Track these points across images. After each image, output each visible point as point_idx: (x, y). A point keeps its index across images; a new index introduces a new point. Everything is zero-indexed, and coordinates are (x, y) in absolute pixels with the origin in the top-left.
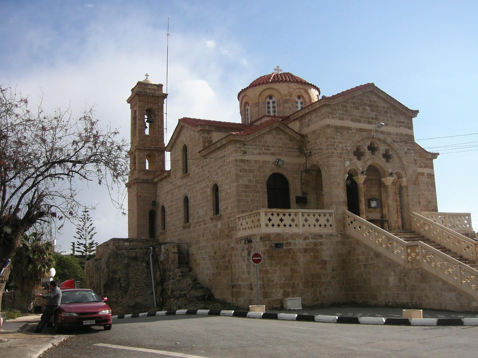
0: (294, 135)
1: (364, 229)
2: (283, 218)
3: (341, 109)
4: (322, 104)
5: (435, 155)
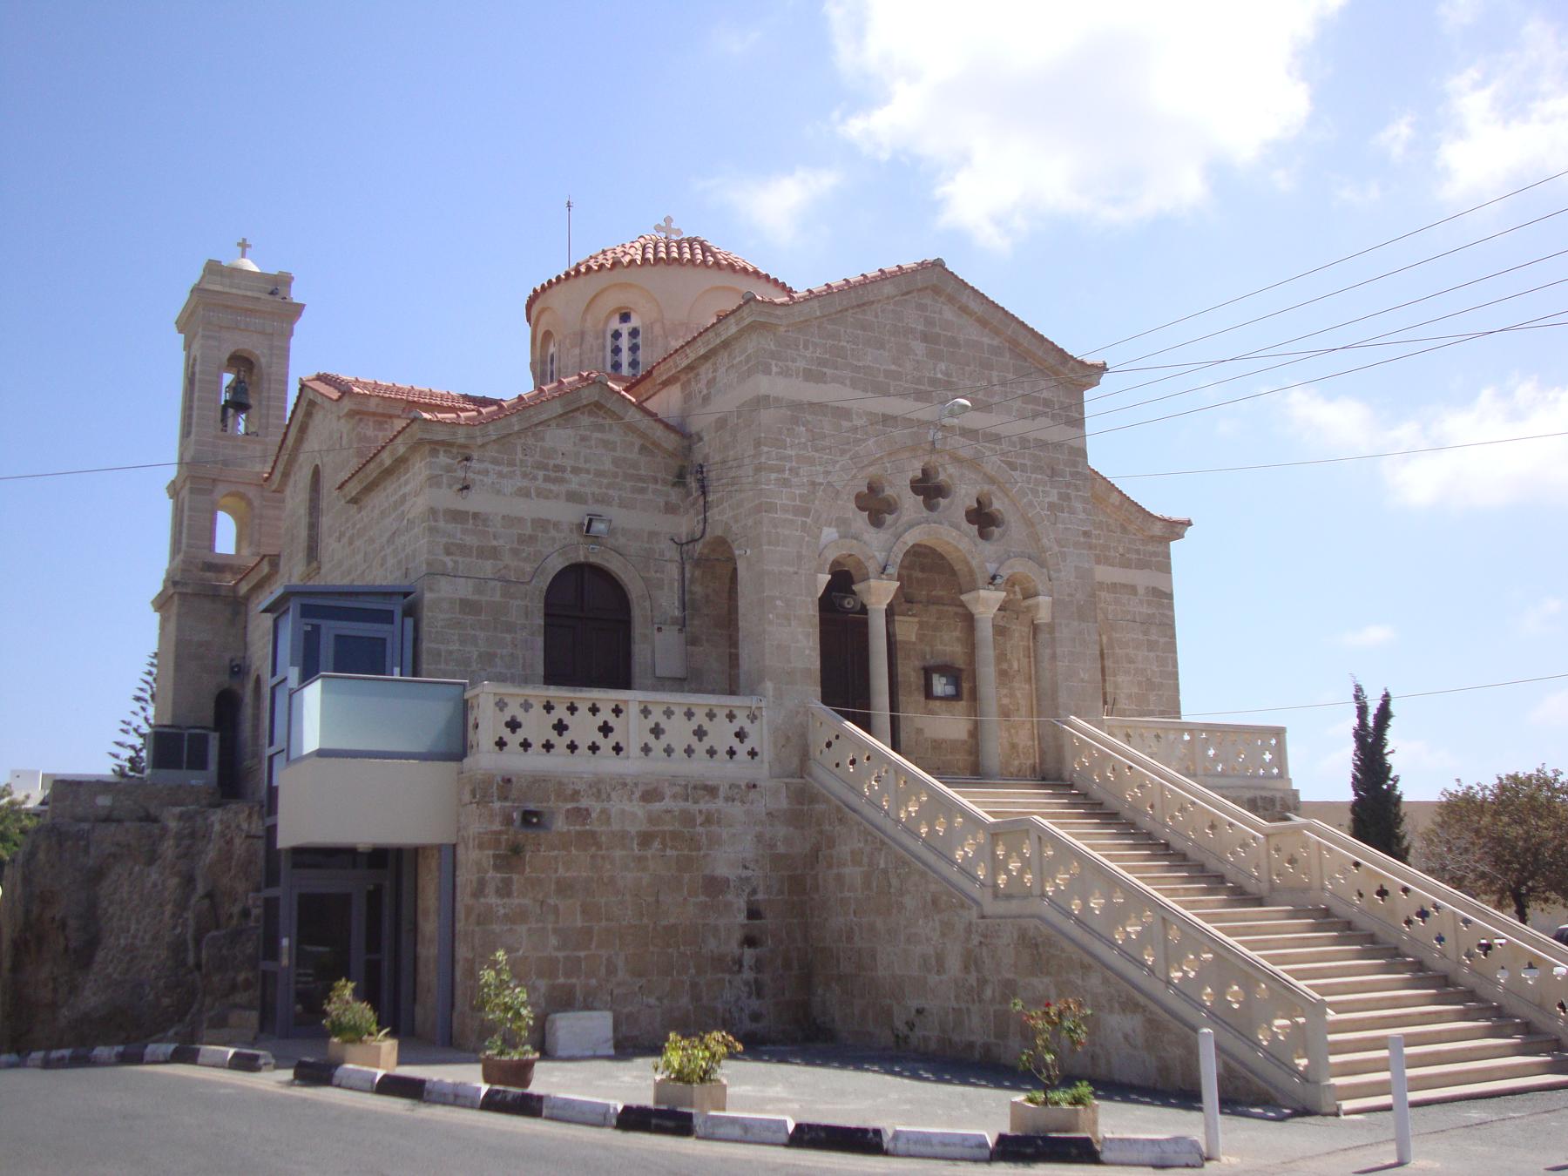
0: (659, 432)
1: (877, 771)
2: (664, 723)
3: (816, 345)
4: (747, 322)
5: (1176, 528)
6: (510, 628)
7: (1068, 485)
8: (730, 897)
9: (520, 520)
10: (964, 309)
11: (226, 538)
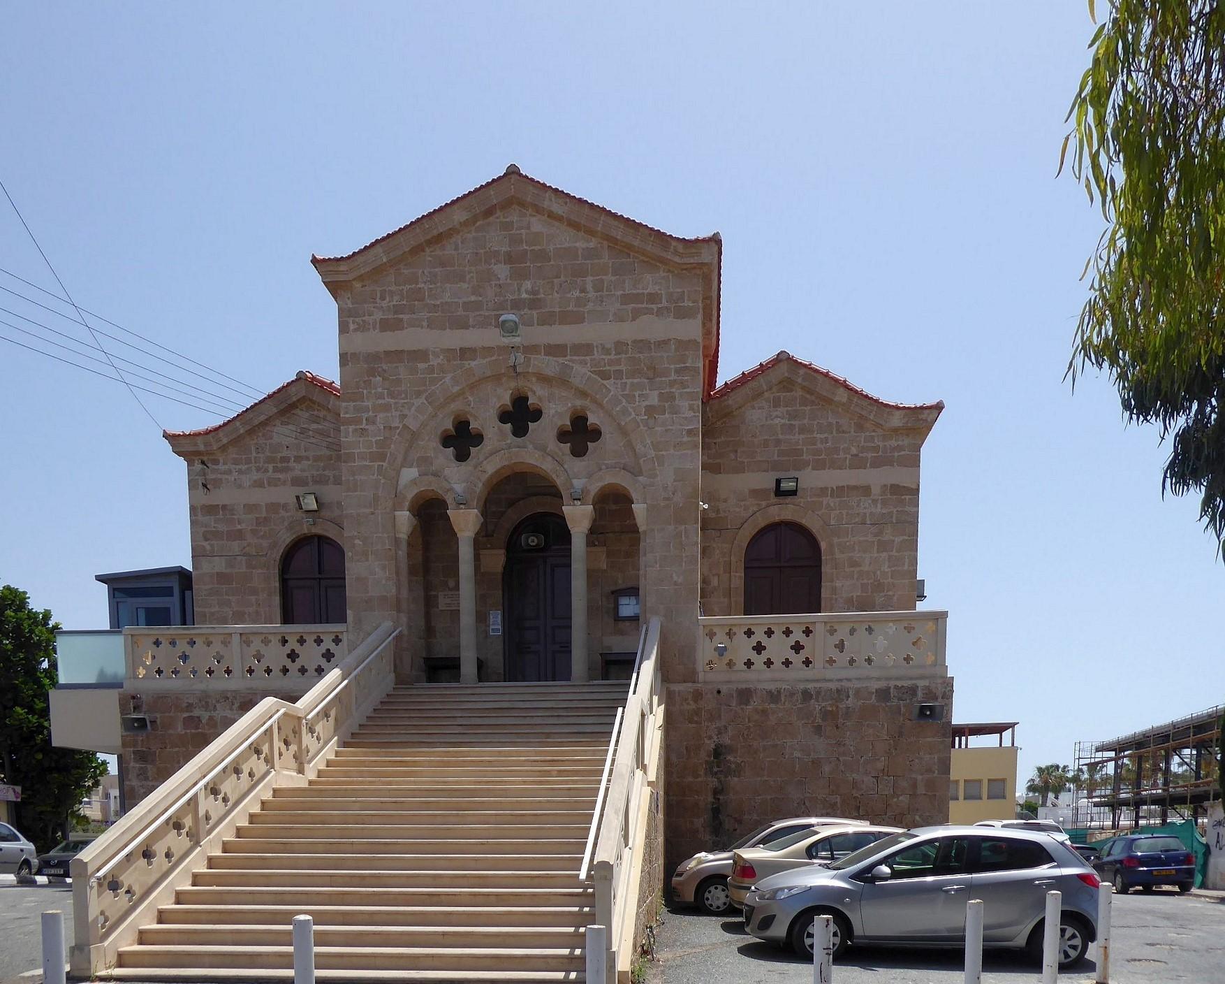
3: (392, 293)
5: (921, 420)
6: (254, 592)
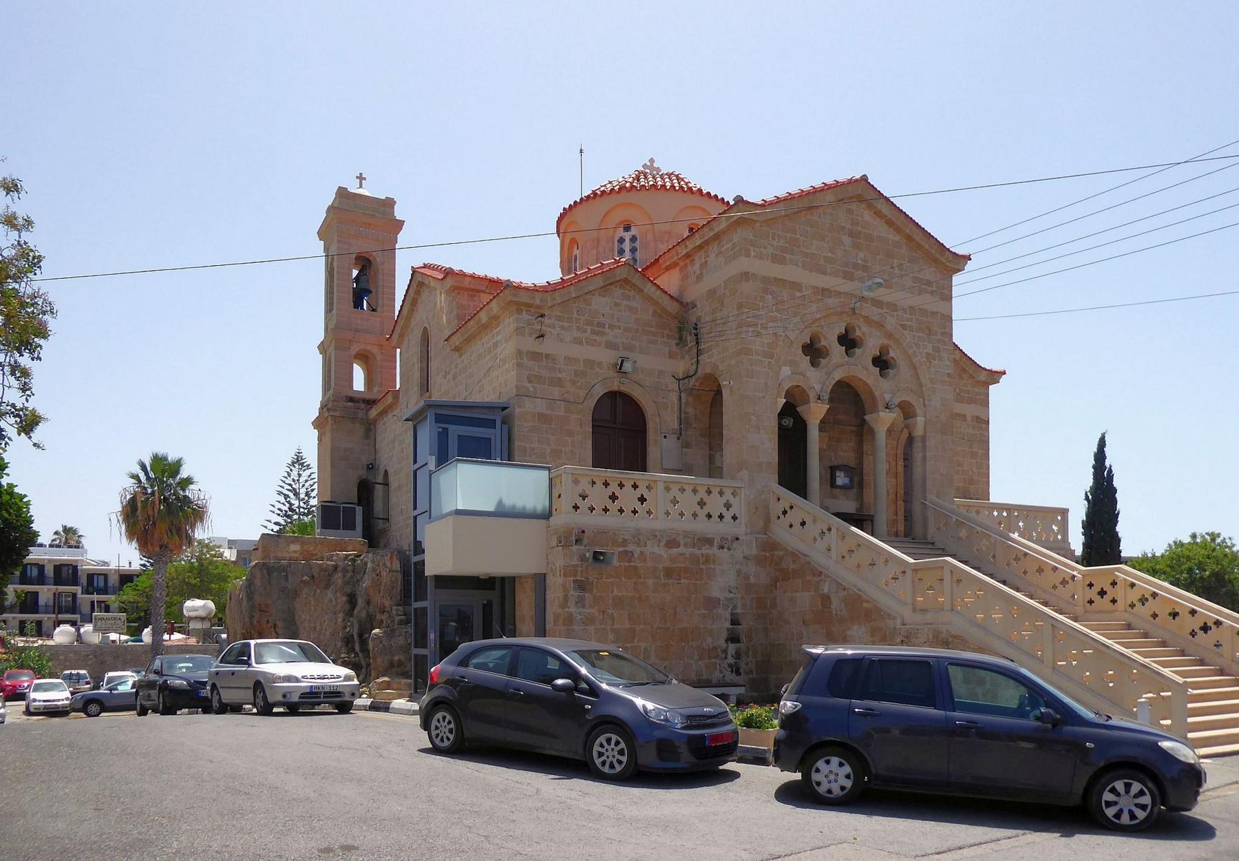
0: (666, 302)
1: (812, 530)
3: (779, 237)
7: (939, 341)
8: (720, 610)
9: (576, 360)
10: (878, 213)
11: (359, 384)
